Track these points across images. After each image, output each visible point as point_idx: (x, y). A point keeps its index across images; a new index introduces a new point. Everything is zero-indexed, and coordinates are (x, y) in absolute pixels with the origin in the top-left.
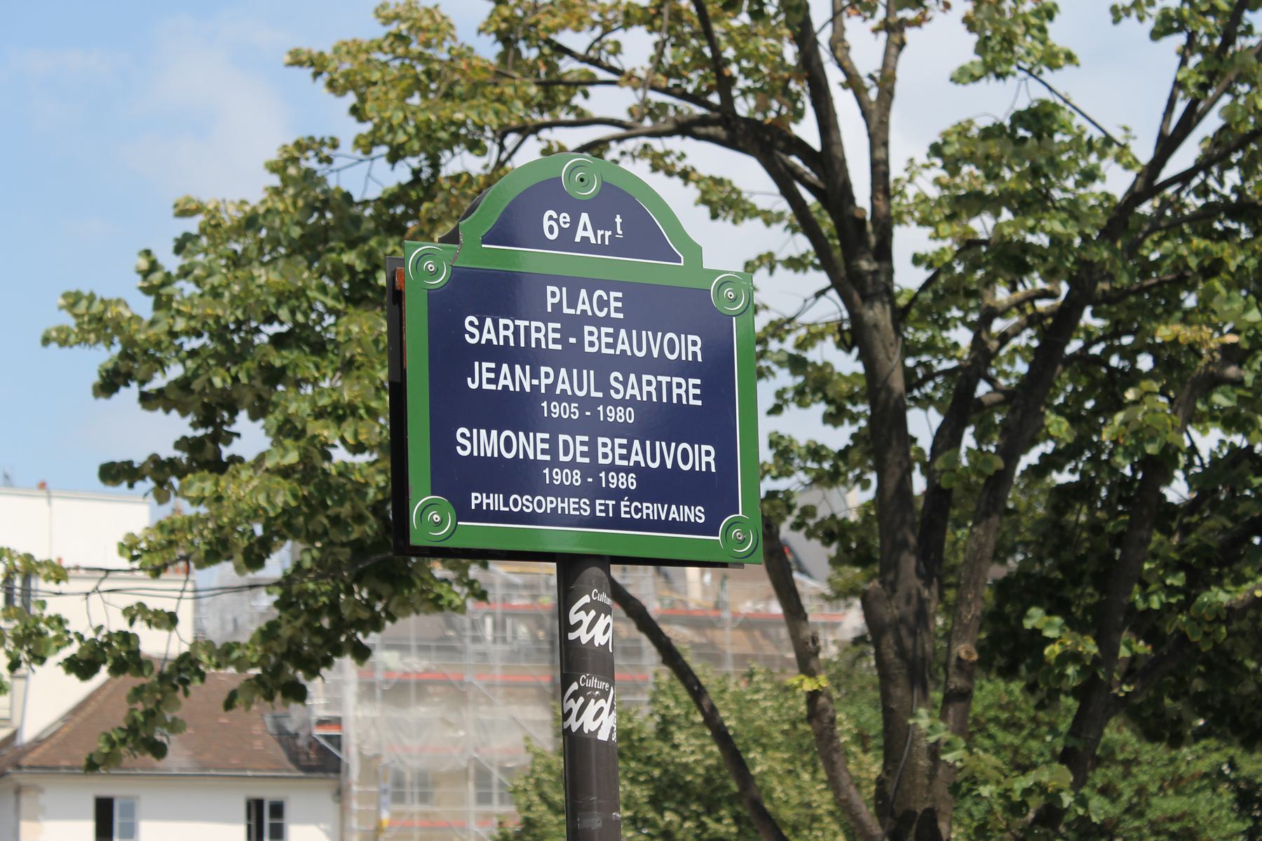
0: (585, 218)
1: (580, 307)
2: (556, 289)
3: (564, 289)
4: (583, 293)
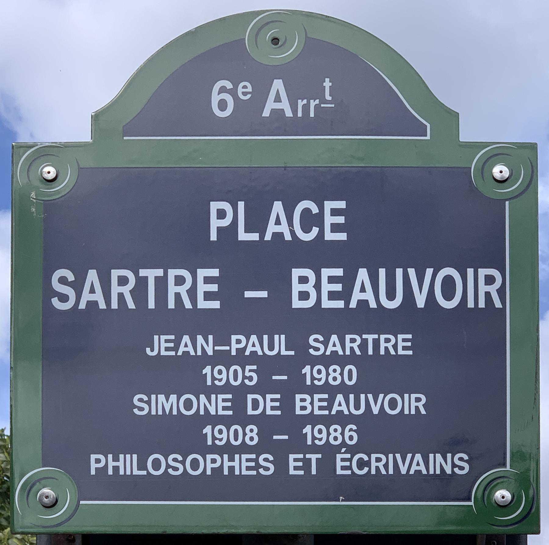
0: (278, 85)
1: (272, 228)
2: (226, 206)
3: (241, 205)
4: (278, 207)
